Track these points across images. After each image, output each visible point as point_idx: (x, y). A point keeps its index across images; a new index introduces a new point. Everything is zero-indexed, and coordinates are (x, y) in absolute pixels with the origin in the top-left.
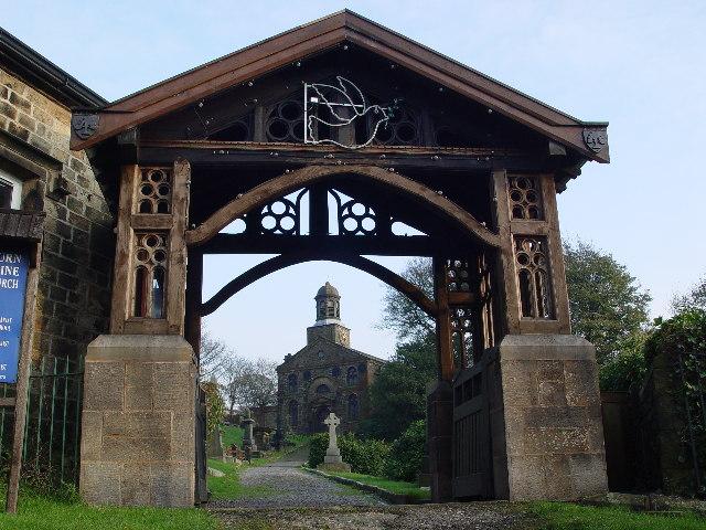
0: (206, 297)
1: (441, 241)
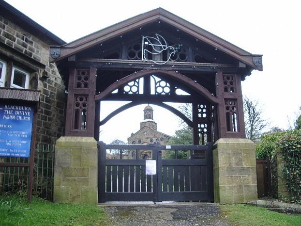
0: (101, 119)
1: (195, 99)
